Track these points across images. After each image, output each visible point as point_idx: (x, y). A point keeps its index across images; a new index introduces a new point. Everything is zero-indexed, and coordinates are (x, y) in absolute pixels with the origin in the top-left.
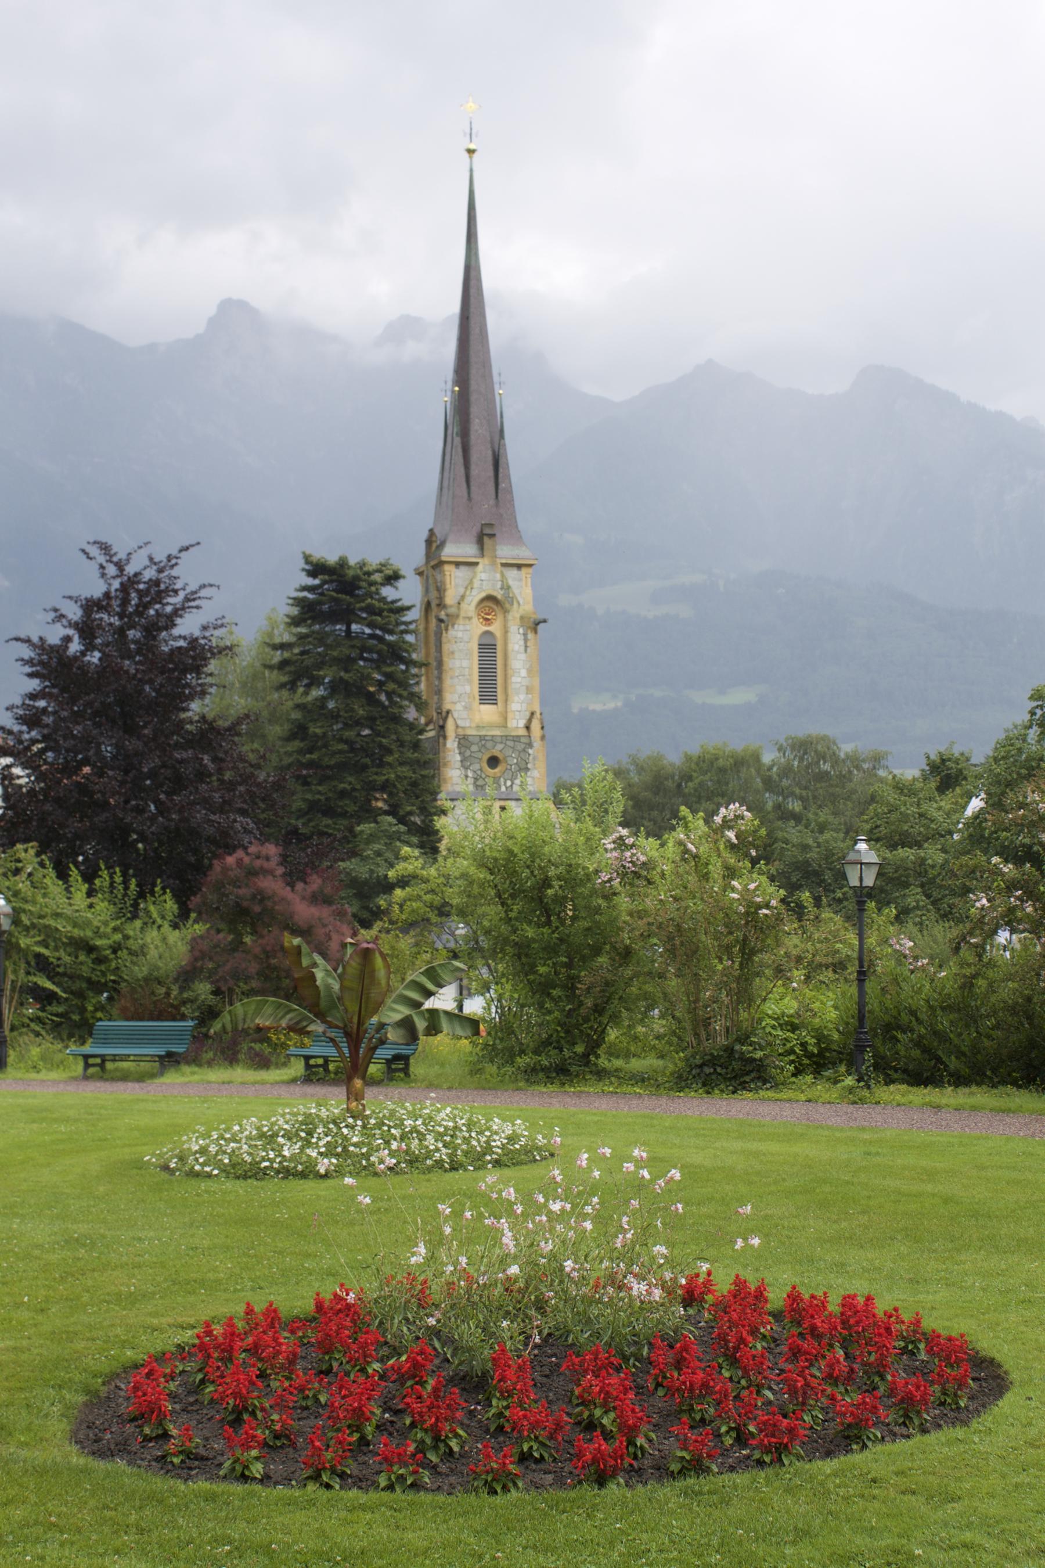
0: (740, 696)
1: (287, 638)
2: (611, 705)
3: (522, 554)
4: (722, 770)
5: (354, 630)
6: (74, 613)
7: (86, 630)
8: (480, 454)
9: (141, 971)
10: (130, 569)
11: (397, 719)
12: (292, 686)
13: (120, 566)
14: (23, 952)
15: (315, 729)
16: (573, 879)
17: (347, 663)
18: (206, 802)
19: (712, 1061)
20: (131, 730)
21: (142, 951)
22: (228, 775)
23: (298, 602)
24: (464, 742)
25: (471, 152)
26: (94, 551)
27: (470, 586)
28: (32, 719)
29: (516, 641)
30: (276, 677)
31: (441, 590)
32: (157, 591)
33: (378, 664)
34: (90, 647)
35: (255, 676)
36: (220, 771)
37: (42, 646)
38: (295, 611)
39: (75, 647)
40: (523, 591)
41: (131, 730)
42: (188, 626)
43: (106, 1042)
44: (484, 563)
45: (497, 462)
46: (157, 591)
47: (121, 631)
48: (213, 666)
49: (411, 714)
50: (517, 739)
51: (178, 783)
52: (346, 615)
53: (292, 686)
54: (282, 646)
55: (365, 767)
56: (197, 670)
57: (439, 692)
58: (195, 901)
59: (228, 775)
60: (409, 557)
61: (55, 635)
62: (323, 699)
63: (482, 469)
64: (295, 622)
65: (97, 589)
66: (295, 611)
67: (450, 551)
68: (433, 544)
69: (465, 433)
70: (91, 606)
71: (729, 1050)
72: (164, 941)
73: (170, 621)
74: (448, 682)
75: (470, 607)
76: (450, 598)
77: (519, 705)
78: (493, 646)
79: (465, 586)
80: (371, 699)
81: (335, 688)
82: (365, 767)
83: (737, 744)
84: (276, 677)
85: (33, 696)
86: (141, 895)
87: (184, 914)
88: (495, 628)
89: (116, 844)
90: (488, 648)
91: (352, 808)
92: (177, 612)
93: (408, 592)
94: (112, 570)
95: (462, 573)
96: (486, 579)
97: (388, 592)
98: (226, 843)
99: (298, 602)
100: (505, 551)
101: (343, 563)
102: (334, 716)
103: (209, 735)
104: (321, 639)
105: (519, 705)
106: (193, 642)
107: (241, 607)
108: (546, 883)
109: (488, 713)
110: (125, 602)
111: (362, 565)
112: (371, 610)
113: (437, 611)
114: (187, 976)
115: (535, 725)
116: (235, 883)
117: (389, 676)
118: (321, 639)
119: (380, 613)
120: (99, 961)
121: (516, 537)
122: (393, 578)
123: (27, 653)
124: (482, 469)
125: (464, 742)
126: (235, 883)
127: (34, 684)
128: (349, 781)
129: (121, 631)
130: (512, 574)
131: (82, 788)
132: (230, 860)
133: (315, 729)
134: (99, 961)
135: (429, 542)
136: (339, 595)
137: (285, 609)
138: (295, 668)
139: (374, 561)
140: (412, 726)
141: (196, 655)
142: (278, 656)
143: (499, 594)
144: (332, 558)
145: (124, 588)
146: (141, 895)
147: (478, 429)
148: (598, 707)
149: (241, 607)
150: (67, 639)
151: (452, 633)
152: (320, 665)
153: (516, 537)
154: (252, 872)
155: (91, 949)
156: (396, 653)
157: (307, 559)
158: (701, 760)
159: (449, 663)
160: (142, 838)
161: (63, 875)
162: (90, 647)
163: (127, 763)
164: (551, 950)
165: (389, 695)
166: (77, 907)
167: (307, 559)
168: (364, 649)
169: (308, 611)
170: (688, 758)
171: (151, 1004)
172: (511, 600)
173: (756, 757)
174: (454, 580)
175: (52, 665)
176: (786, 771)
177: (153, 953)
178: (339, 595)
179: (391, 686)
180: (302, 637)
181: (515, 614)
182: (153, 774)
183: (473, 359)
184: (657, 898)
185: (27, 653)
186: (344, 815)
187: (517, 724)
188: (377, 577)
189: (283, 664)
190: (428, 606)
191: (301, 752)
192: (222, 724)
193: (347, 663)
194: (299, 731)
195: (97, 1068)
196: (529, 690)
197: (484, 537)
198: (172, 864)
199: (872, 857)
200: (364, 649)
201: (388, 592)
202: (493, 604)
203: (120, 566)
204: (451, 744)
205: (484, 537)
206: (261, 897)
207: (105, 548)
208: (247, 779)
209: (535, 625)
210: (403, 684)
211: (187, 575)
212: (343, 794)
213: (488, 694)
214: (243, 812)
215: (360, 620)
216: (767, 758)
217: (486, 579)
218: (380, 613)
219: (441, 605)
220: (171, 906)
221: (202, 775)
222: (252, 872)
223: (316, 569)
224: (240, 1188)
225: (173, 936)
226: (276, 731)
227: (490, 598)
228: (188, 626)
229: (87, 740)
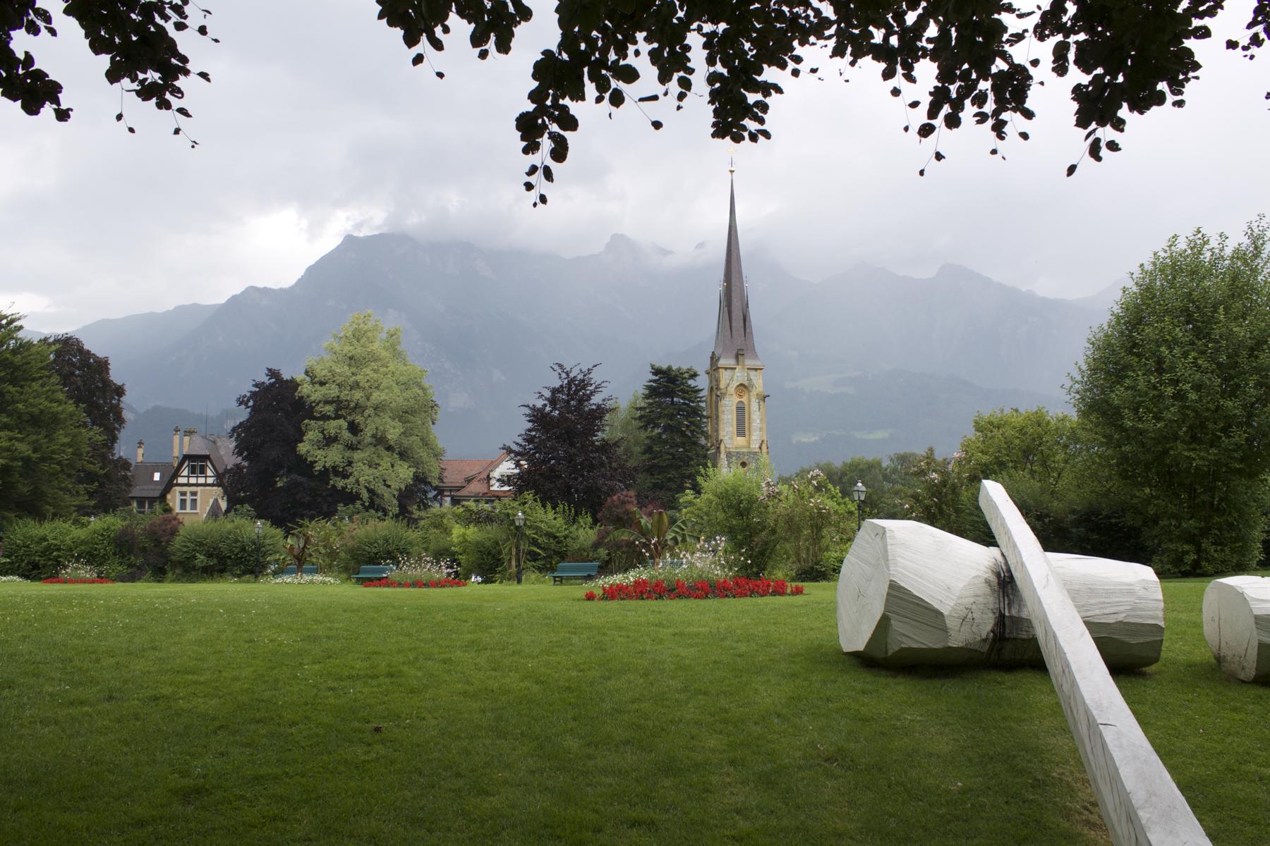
0: (879, 435)
1: (643, 405)
2: (813, 439)
3: (756, 363)
4: (862, 470)
5: (676, 404)
6: (548, 394)
7: (553, 401)
8: (737, 315)
9: (576, 546)
10: (572, 375)
11: (695, 444)
12: (645, 427)
13: (567, 374)
14: (528, 537)
15: (656, 448)
16: (752, 500)
17: (671, 417)
18: (604, 476)
19: (805, 572)
20: (572, 444)
21: (577, 537)
22: (614, 465)
23: (648, 387)
24: (729, 455)
25: (732, 172)
26: (556, 367)
27: (732, 379)
28: (530, 440)
29: (754, 405)
30: (636, 423)
31: (718, 381)
32: (583, 384)
33: (687, 417)
34: (554, 409)
35: (627, 423)
36: (610, 463)
37: (534, 408)
38: (647, 392)
39: (548, 409)
40: (758, 381)
41: (572, 444)
42: (596, 399)
43: (563, 571)
44: (739, 368)
45: (745, 319)
46: (583, 384)
47: (568, 402)
48: (607, 417)
49: (703, 441)
50: (755, 453)
51: (592, 467)
52: (671, 394)
53: (645, 427)
54: (641, 409)
55: (680, 467)
56: (601, 418)
57: (717, 431)
58: (599, 515)
59: (614, 465)
60: (702, 366)
61: (539, 403)
62: (660, 434)
63: (737, 323)
64: (647, 397)
65: (557, 384)
66: (647, 392)
67: (722, 363)
68: (714, 359)
69: (729, 305)
70: (555, 391)
71: (812, 568)
72: (585, 533)
73: (589, 397)
74: (721, 426)
75: (732, 389)
76: (722, 385)
77: (756, 437)
78: (743, 408)
79: (730, 379)
80: (683, 434)
81: (666, 429)
82: (680, 467)
83: (870, 457)
84: (636, 423)
85: (530, 430)
86: (576, 515)
87: (595, 521)
88: (744, 399)
89: (566, 494)
90: (741, 409)
91: (674, 486)
92: (592, 393)
93: (702, 382)
94: (564, 375)
95: (728, 373)
96: (740, 376)
97: (690, 382)
98: (612, 491)
99: (648, 387)
100: (749, 362)
101: (670, 369)
102: (665, 442)
103: (606, 447)
104: (659, 405)
105: (756, 437)
106: (599, 406)
107: (621, 388)
108: (741, 502)
109: (741, 441)
110: (570, 389)
111: (679, 369)
112: (683, 391)
113: (715, 388)
114: (596, 546)
115: (764, 447)
116: (617, 507)
117: (691, 423)
118: (659, 405)
119: (687, 392)
120: (558, 542)
121: (755, 356)
122: (694, 376)
123: (528, 411)
124: (737, 323)
125: (729, 455)
126: (617, 507)
127: (530, 425)
128: (672, 474)
129: (568, 402)
130: (752, 373)
131: (552, 469)
132: (615, 498)
133: (656, 448)
134: (558, 542)
135: (712, 358)
136: (668, 384)
137: (642, 391)
138: (646, 419)
139: (685, 368)
140: (703, 447)
141: (600, 412)
142: (639, 414)
143: (746, 383)
144: (664, 367)
145: (569, 383)
146: (576, 515)
147: (736, 304)
148: (806, 440)
149: (621, 388)
150: (545, 405)
151: (723, 402)
152: (659, 418)
153: (755, 356)
154: (624, 503)
155: (555, 537)
156: (695, 412)
157: (652, 367)
158: (851, 465)
159: (722, 416)
160: (577, 491)
161: (544, 506)
162: (554, 409)
163: (570, 459)
164: (743, 530)
165: (692, 432)
166: (550, 519)
167: (652, 367)
168: (680, 410)
169: (653, 392)
170: (845, 464)
171: (581, 556)
172: (752, 386)
173: (879, 464)
174: (724, 376)
175: (538, 417)
176: (895, 471)
177: (582, 538)
178: (668, 384)
179: (693, 428)
180: (650, 404)
181: (754, 393)
182: (581, 463)
183: (733, 270)
184: (782, 508)
185: (528, 411)
186: (670, 490)
187: (755, 446)
188: (686, 375)
189: (641, 418)
190: (712, 389)
191: (649, 459)
192: (611, 442)
193: (671, 417)
194: (649, 449)
195: (559, 581)
196: (761, 429)
197: (738, 356)
198: (589, 502)
199: (864, 489)
200: (680, 410)
201: (690, 382)
202: (743, 388)
203: (567, 374)
204: (723, 456)
205: (738, 356)
206: (628, 512)
207: (561, 366)
208: (622, 467)
209: (764, 398)
210: (699, 427)
211: (596, 377)
212: (669, 480)
213: (741, 431)
214: (620, 481)
215: (678, 396)
216: (884, 465)
217: (740, 376)
218: (687, 392)
219: (718, 389)
220: (589, 519)
221: (602, 464)
222: (624, 503)
223: (657, 371)
224: (614, 604)
225: (590, 532)
226: (638, 449)
227: (741, 385)
228: (596, 399)
229: (554, 449)
